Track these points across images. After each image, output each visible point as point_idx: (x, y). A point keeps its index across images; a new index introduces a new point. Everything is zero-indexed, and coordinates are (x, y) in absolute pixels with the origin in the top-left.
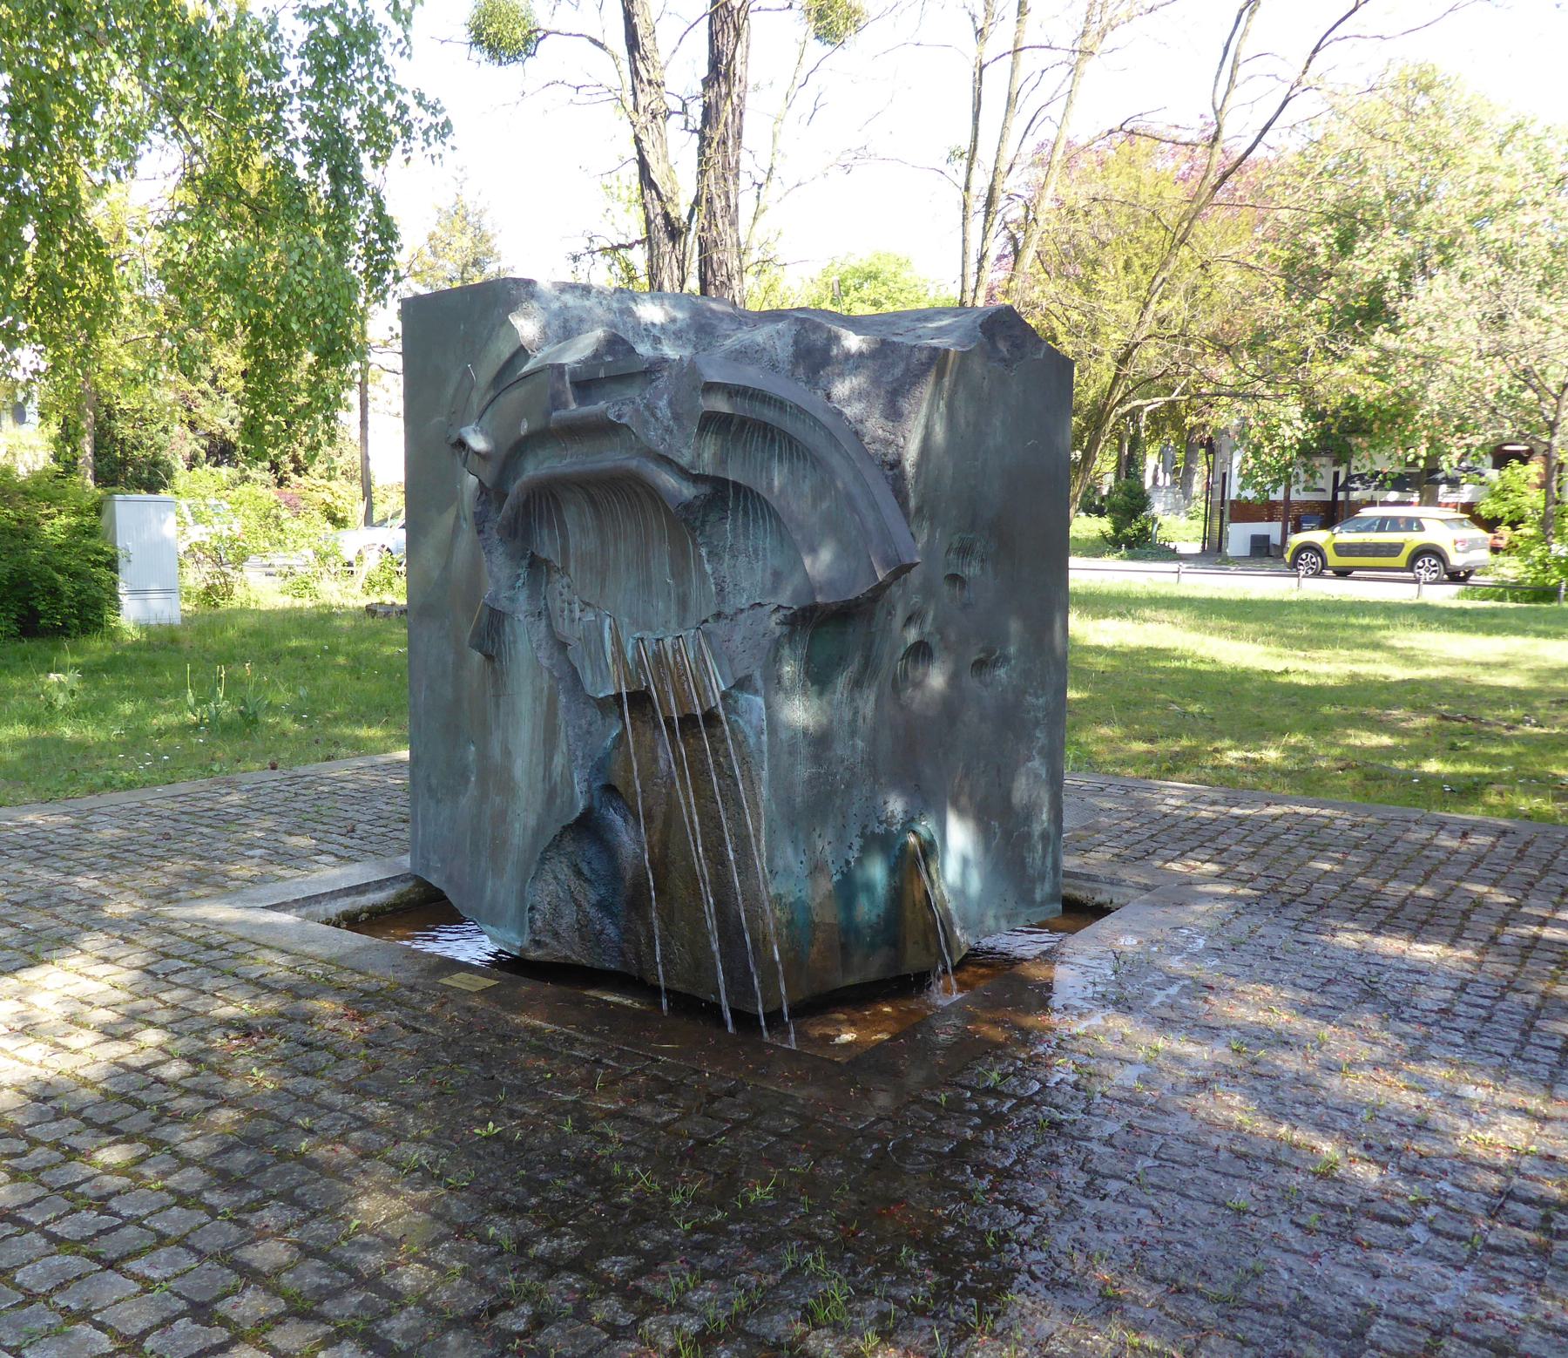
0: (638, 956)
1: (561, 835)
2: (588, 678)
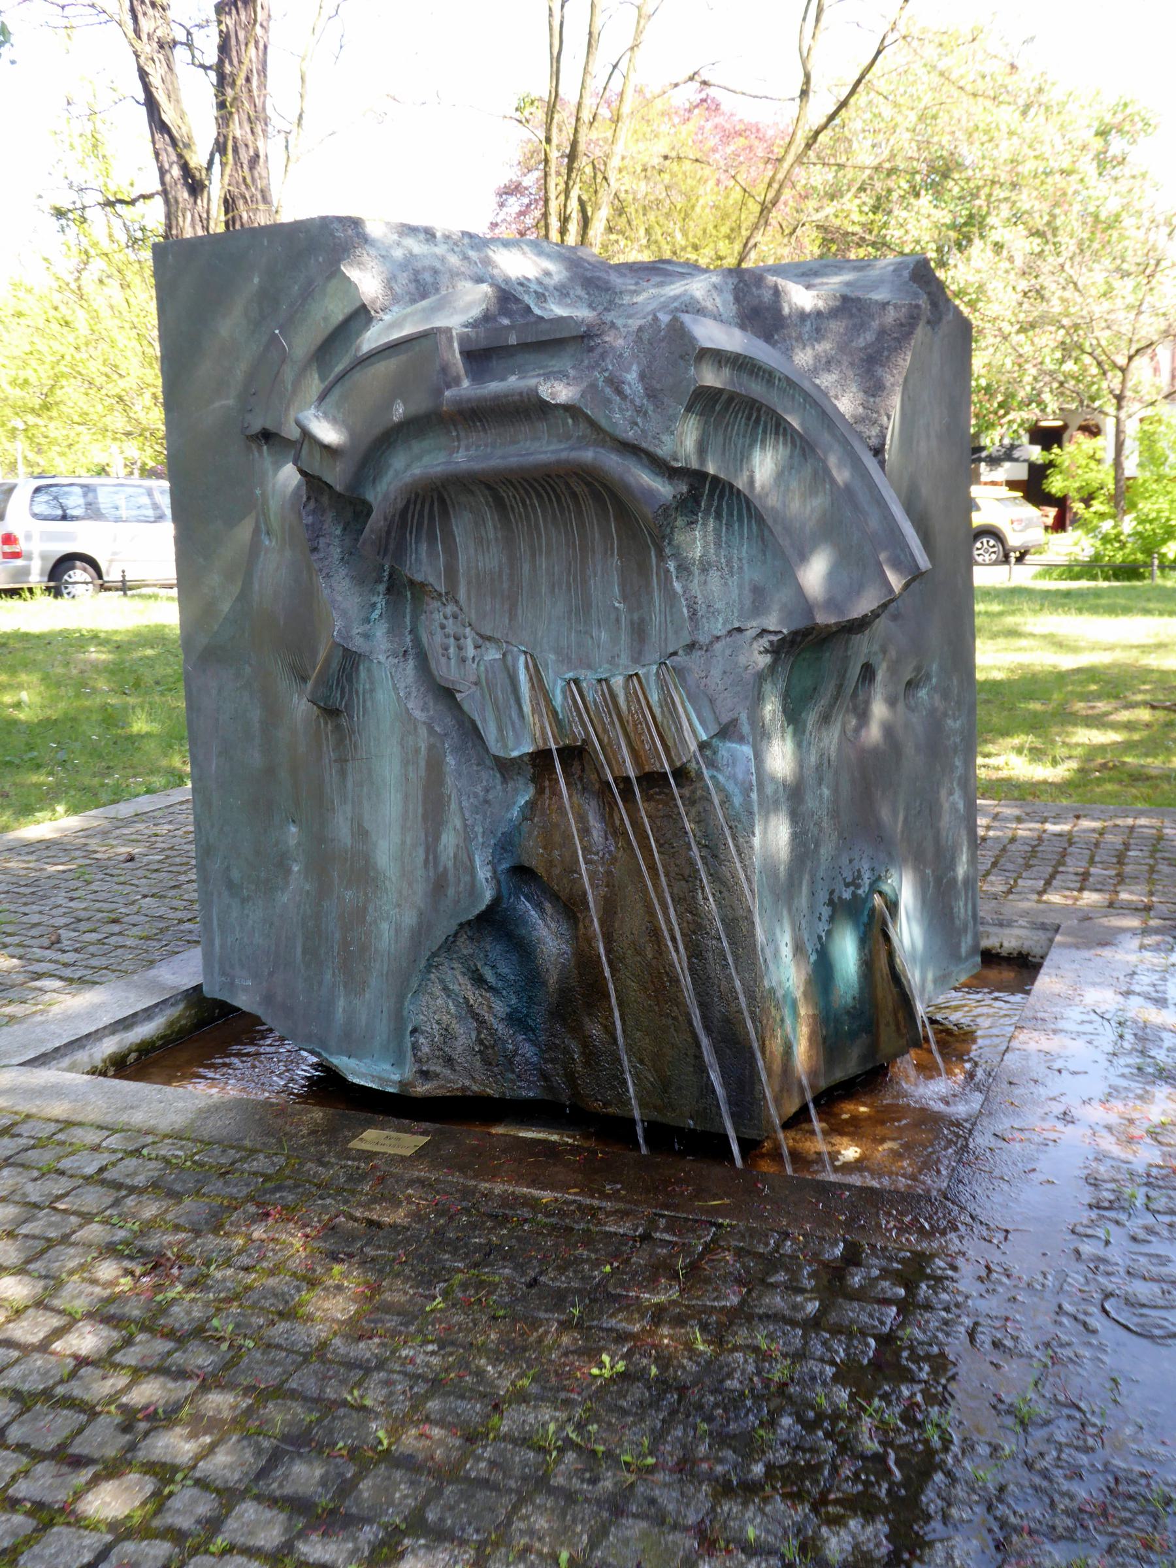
0: (571, 1078)
1: (456, 935)
2: (490, 733)
